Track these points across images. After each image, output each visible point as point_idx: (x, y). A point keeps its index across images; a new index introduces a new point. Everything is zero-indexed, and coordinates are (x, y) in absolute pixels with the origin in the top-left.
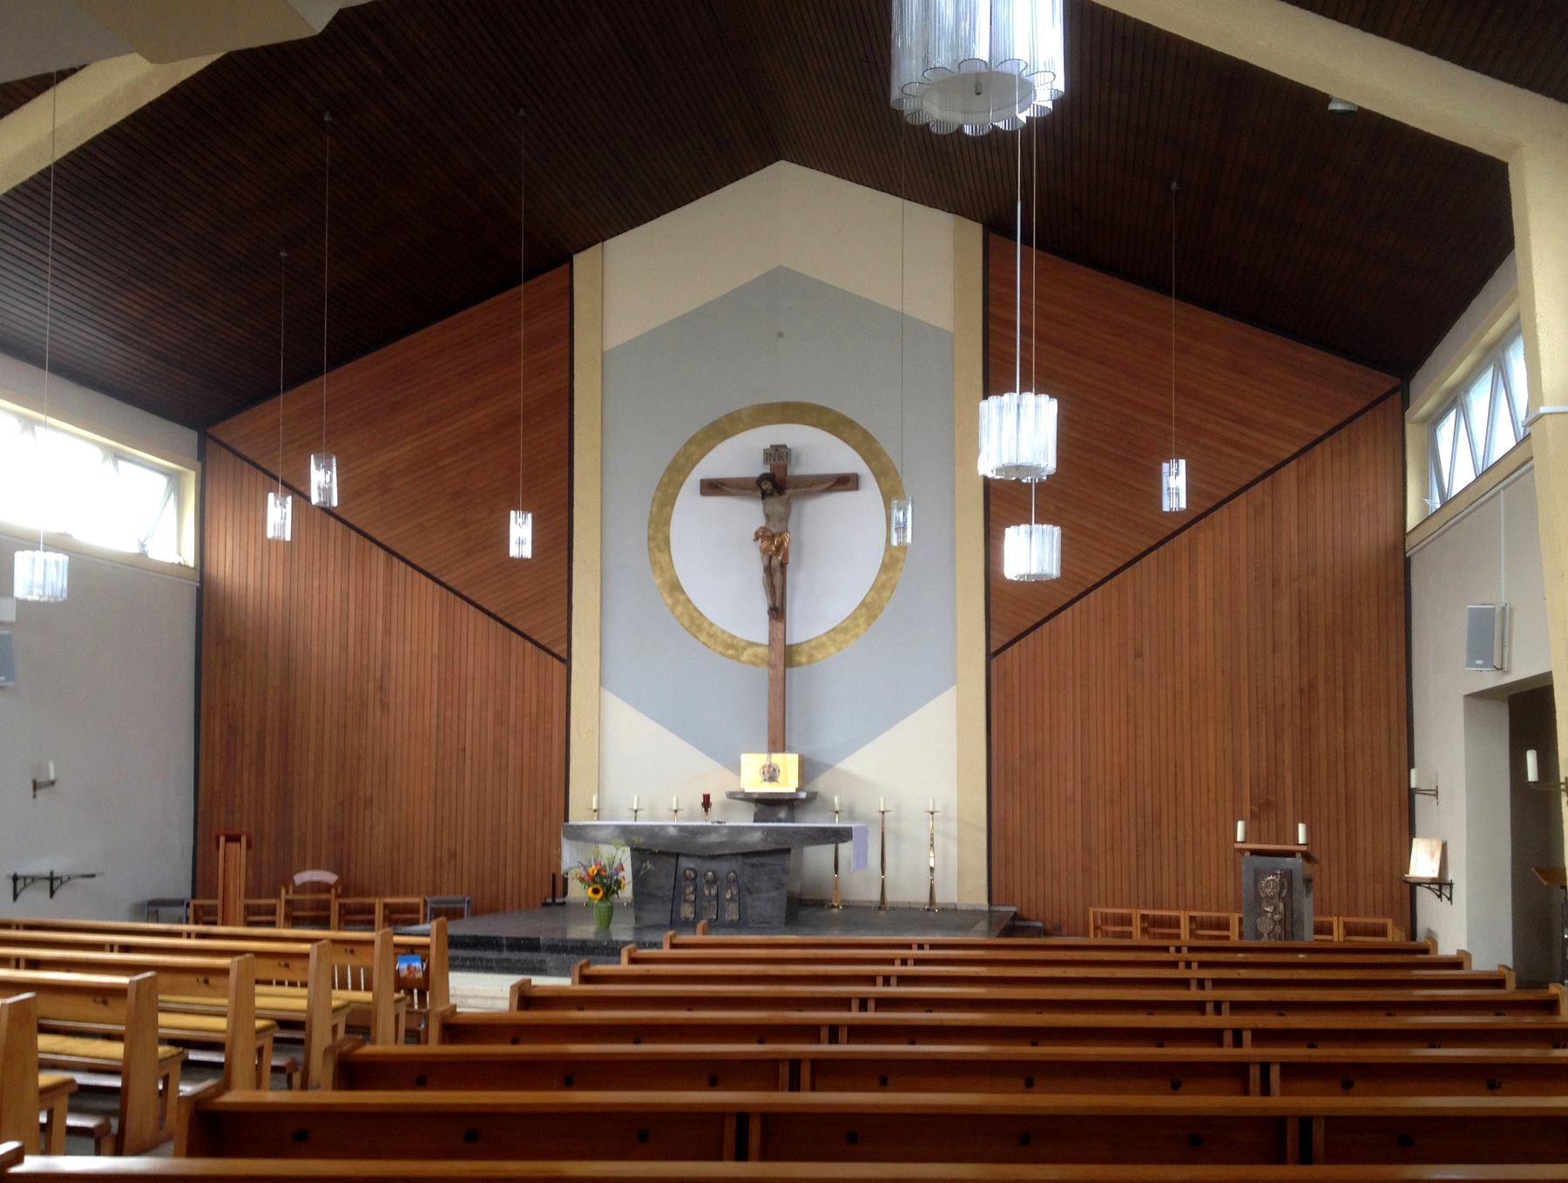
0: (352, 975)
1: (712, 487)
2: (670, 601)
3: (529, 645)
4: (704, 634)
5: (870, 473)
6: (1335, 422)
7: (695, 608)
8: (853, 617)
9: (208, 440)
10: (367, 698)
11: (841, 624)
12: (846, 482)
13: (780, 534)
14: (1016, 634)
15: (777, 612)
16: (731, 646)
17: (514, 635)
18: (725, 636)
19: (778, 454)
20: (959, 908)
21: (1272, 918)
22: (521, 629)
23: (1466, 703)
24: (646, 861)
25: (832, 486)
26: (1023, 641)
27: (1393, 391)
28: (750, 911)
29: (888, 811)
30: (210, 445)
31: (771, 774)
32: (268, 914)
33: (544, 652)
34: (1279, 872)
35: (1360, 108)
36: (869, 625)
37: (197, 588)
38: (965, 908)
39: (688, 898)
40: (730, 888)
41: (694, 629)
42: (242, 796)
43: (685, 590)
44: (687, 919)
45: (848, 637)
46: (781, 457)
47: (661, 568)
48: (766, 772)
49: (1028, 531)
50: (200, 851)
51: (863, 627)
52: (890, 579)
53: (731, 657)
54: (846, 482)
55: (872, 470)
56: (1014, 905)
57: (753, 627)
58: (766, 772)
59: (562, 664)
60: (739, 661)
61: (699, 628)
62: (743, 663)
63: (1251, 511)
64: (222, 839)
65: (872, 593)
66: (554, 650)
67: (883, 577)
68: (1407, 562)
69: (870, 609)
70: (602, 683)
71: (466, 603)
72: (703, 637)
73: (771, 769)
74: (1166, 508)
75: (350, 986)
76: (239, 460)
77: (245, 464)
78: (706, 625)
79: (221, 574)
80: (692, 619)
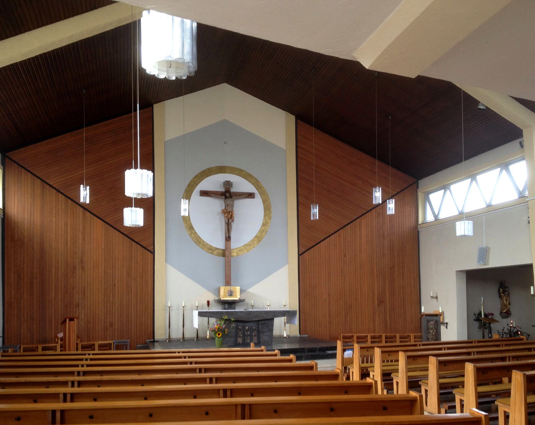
0: (370, 360)
1: (204, 193)
2: (189, 232)
3: (139, 246)
4: (201, 244)
5: (258, 192)
6: (399, 190)
7: (198, 236)
8: (253, 241)
9: (6, 159)
10: (76, 265)
11: (248, 243)
12: (251, 195)
13: (232, 212)
14: (308, 248)
15: (228, 239)
16: (210, 249)
17: (133, 243)
18: (208, 246)
19: (228, 184)
20: (290, 336)
21: (432, 334)
22: (136, 240)
23: (456, 274)
24: (233, 323)
25: (246, 196)
26: (310, 251)
27: (413, 183)
28: (261, 339)
29: (270, 305)
30: (7, 159)
31: (231, 294)
32: (378, 338)
33: (145, 250)
34: (434, 321)
35: (487, 108)
36: (258, 244)
37: (2, 218)
38: (292, 336)
39: (240, 336)
40: (254, 332)
41: (198, 243)
42: (24, 303)
43: (194, 229)
44: (239, 343)
45: (251, 247)
46: (229, 185)
47: (186, 221)
48: (229, 293)
49: (131, 210)
50: (6, 326)
51: (256, 244)
52: (265, 229)
53: (210, 253)
54: (251, 195)
55: (259, 192)
56: (307, 335)
57: (220, 244)
58: (229, 293)
59: (151, 254)
60: (213, 254)
61: (200, 242)
62: (214, 255)
63: (377, 215)
64: (68, 320)
65: (259, 233)
66: (148, 249)
67: (263, 228)
68: (418, 232)
69: (258, 238)
70: (166, 261)
71: (115, 230)
72: (201, 246)
73: (231, 292)
74: (388, 214)
75: (369, 362)
76: (20, 168)
77: (23, 170)
78: (202, 241)
79: (13, 213)
80: (197, 239)
